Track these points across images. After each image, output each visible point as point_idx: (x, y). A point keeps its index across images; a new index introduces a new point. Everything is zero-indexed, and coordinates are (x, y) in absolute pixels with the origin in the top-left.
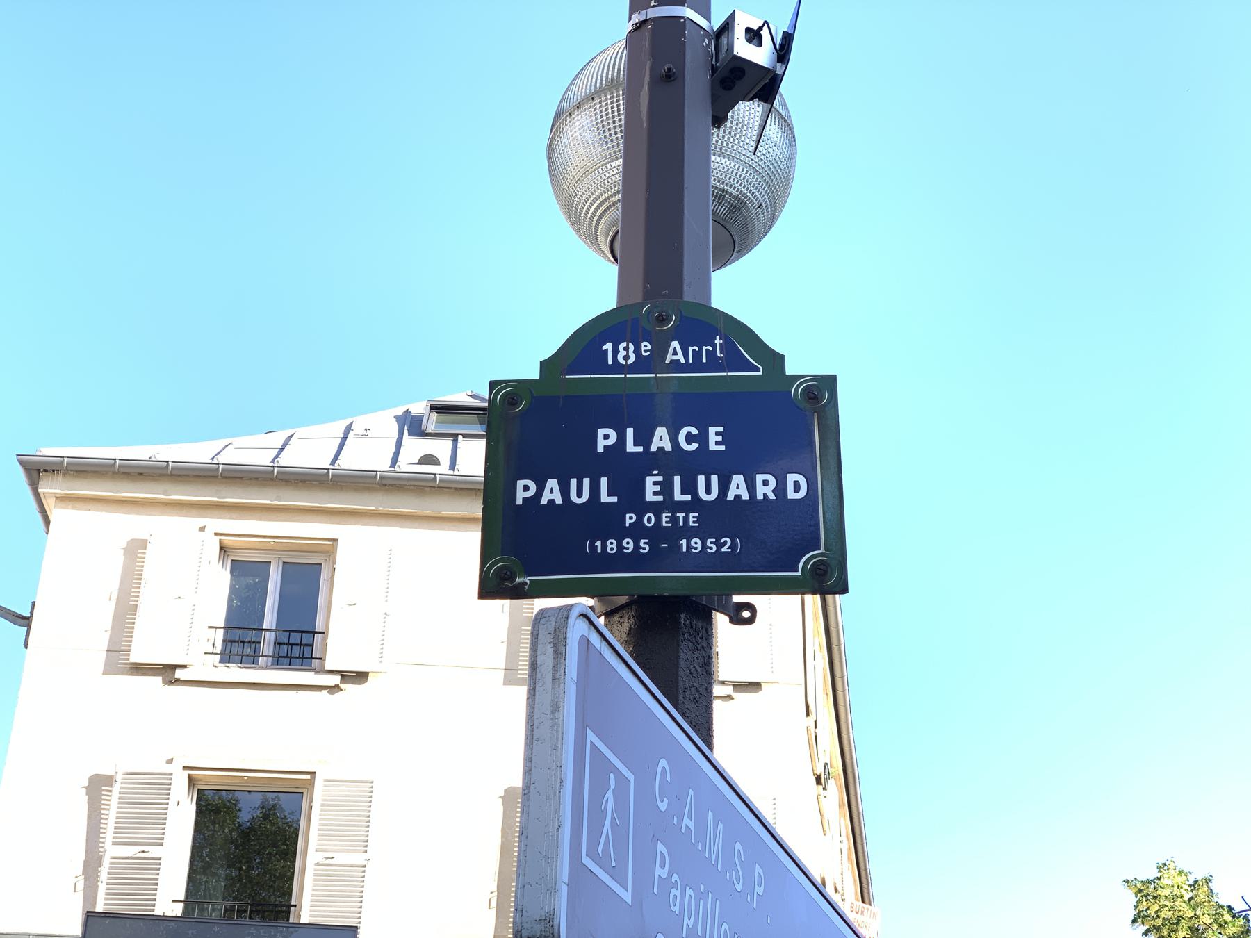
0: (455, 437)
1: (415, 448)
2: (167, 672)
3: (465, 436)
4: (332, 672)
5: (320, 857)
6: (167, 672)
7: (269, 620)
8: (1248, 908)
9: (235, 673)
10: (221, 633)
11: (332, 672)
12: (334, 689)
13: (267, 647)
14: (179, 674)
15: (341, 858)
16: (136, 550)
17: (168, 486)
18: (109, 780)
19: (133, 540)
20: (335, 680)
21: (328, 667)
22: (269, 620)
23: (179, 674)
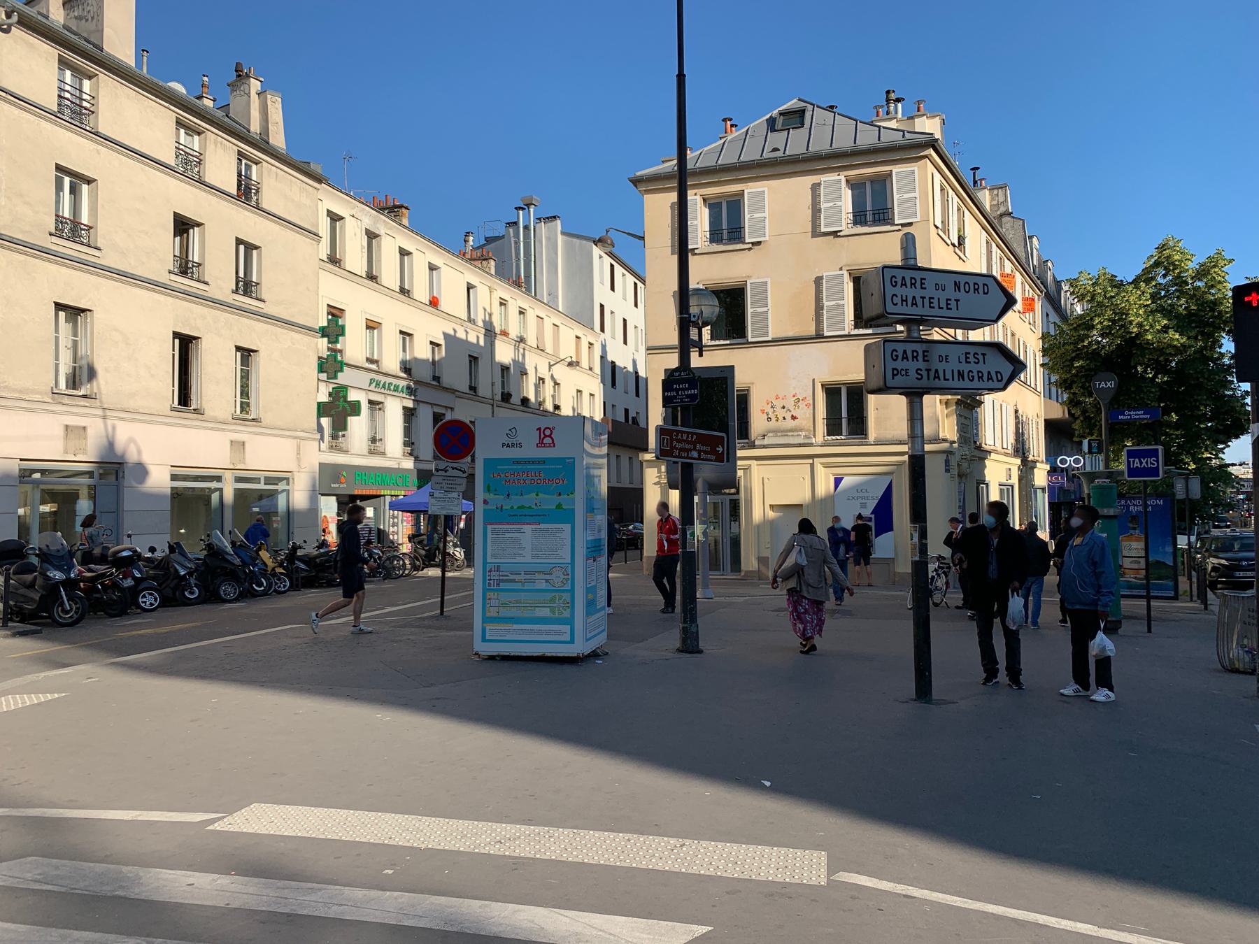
0: (789, 129)
1: (777, 139)
2: (835, 234)
3: (793, 128)
4: (897, 225)
5: (752, 310)
6: (835, 234)
7: (725, 226)
8: (953, 335)
9: (716, 247)
10: (708, 233)
11: (897, 225)
12: (750, 249)
13: (725, 236)
14: (696, 251)
15: (759, 310)
16: (815, 188)
17: (737, 173)
18: (821, 278)
19: (813, 184)
20: (900, 227)
21: (746, 242)
22: (725, 226)
23: (696, 251)
